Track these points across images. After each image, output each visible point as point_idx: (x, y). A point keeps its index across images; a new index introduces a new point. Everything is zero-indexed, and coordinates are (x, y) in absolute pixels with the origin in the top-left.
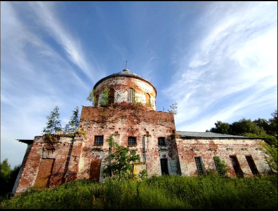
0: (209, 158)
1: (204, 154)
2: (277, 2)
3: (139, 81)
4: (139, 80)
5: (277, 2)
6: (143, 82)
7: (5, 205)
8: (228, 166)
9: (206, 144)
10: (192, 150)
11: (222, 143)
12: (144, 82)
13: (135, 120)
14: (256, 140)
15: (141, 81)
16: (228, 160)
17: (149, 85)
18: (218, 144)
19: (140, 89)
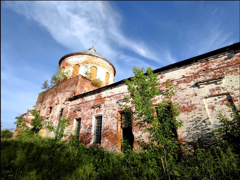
0: (89, 119)
1: (86, 114)
2: (1, 1)
3: (70, 58)
4: (70, 57)
5: (1, 1)
6: (99, 53)
7: (17, 164)
8: (111, 128)
9: (91, 101)
10: (74, 111)
11: (113, 93)
12: (75, 56)
13: (235, 131)
14: (204, 60)
15: (72, 57)
16: (114, 119)
17: (81, 56)
18: (106, 96)
19: (69, 65)
